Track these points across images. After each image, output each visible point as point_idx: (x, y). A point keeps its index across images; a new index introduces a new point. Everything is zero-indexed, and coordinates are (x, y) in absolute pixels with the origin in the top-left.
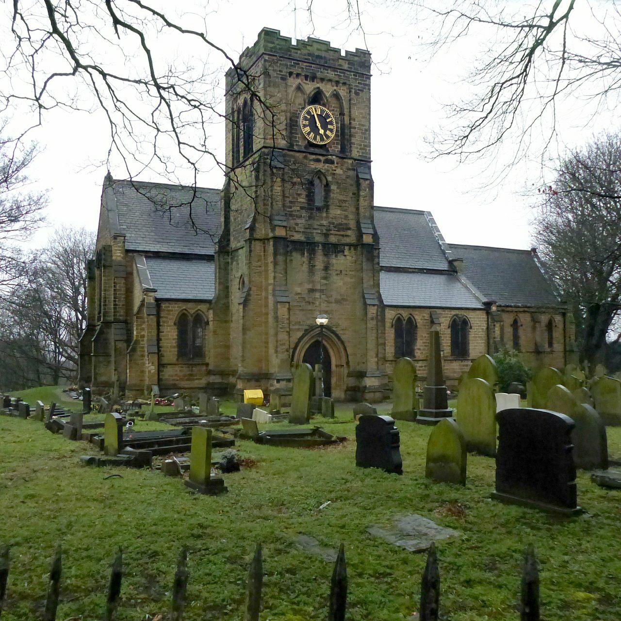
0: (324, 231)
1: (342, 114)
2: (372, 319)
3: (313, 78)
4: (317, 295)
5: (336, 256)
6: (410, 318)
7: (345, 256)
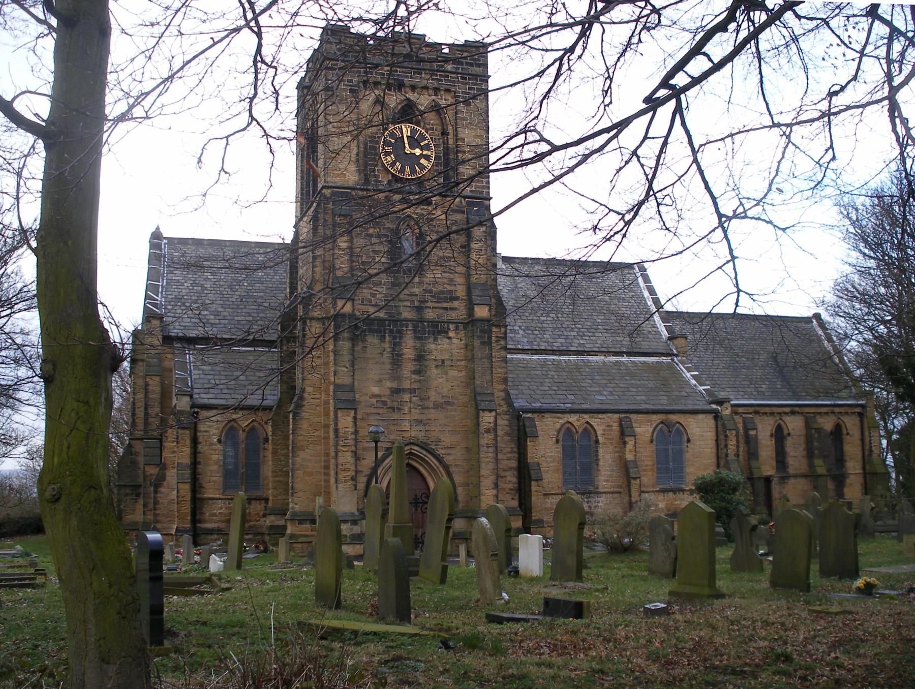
0: (416, 304)
1: (444, 133)
2: (488, 431)
3: (400, 86)
4: (406, 397)
5: (435, 339)
6: (585, 429)
7: (450, 338)
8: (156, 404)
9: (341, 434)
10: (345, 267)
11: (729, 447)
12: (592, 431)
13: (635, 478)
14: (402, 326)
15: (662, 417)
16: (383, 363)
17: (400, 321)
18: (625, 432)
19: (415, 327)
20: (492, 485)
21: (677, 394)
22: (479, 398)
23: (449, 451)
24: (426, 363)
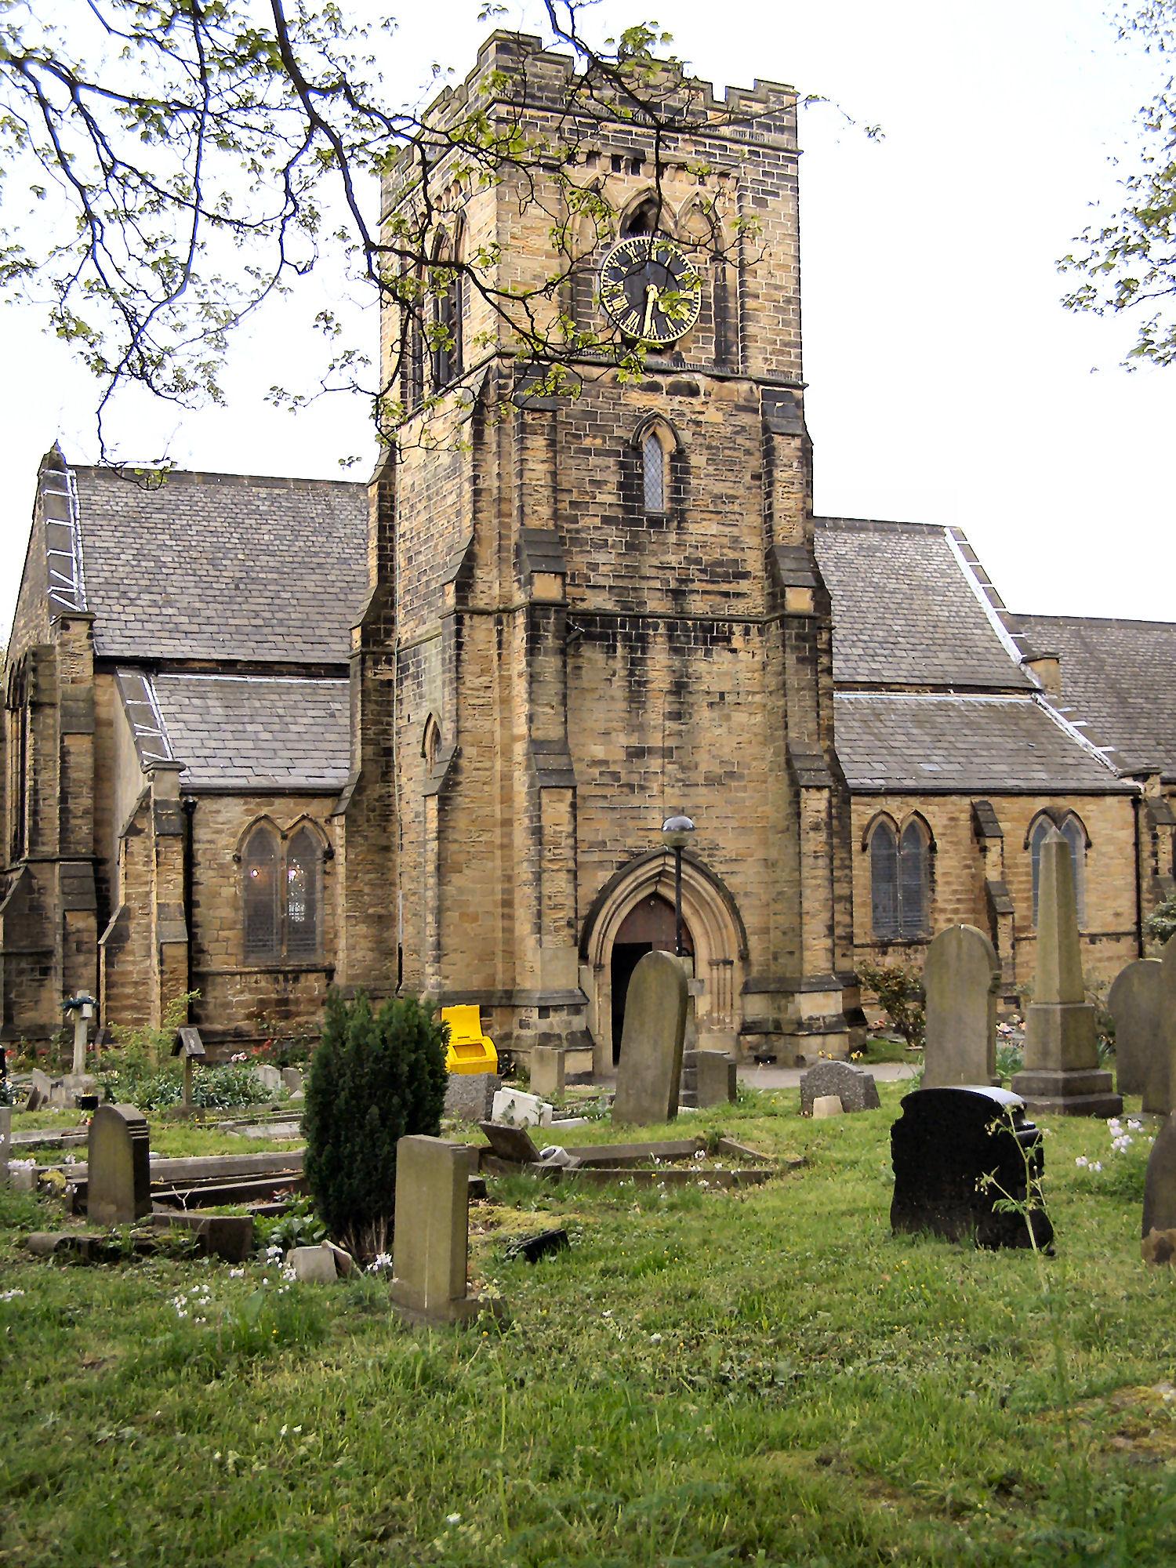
0: (673, 585)
2: (816, 828)
4: (655, 764)
5: (708, 653)
6: (912, 825)
7: (734, 651)
8: (85, 790)
9: (546, 838)
10: (545, 511)
11: (1161, 856)
12: (1077, 824)
13: (1004, 914)
14: (646, 626)
15: (1042, 803)
16: (612, 698)
17: (644, 617)
18: (981, 829)
19: (671, 628)
20: (824, 931)
21: (1059, 760)
22: (797, 765)
23: (734, 867)
24: (691, 699)
